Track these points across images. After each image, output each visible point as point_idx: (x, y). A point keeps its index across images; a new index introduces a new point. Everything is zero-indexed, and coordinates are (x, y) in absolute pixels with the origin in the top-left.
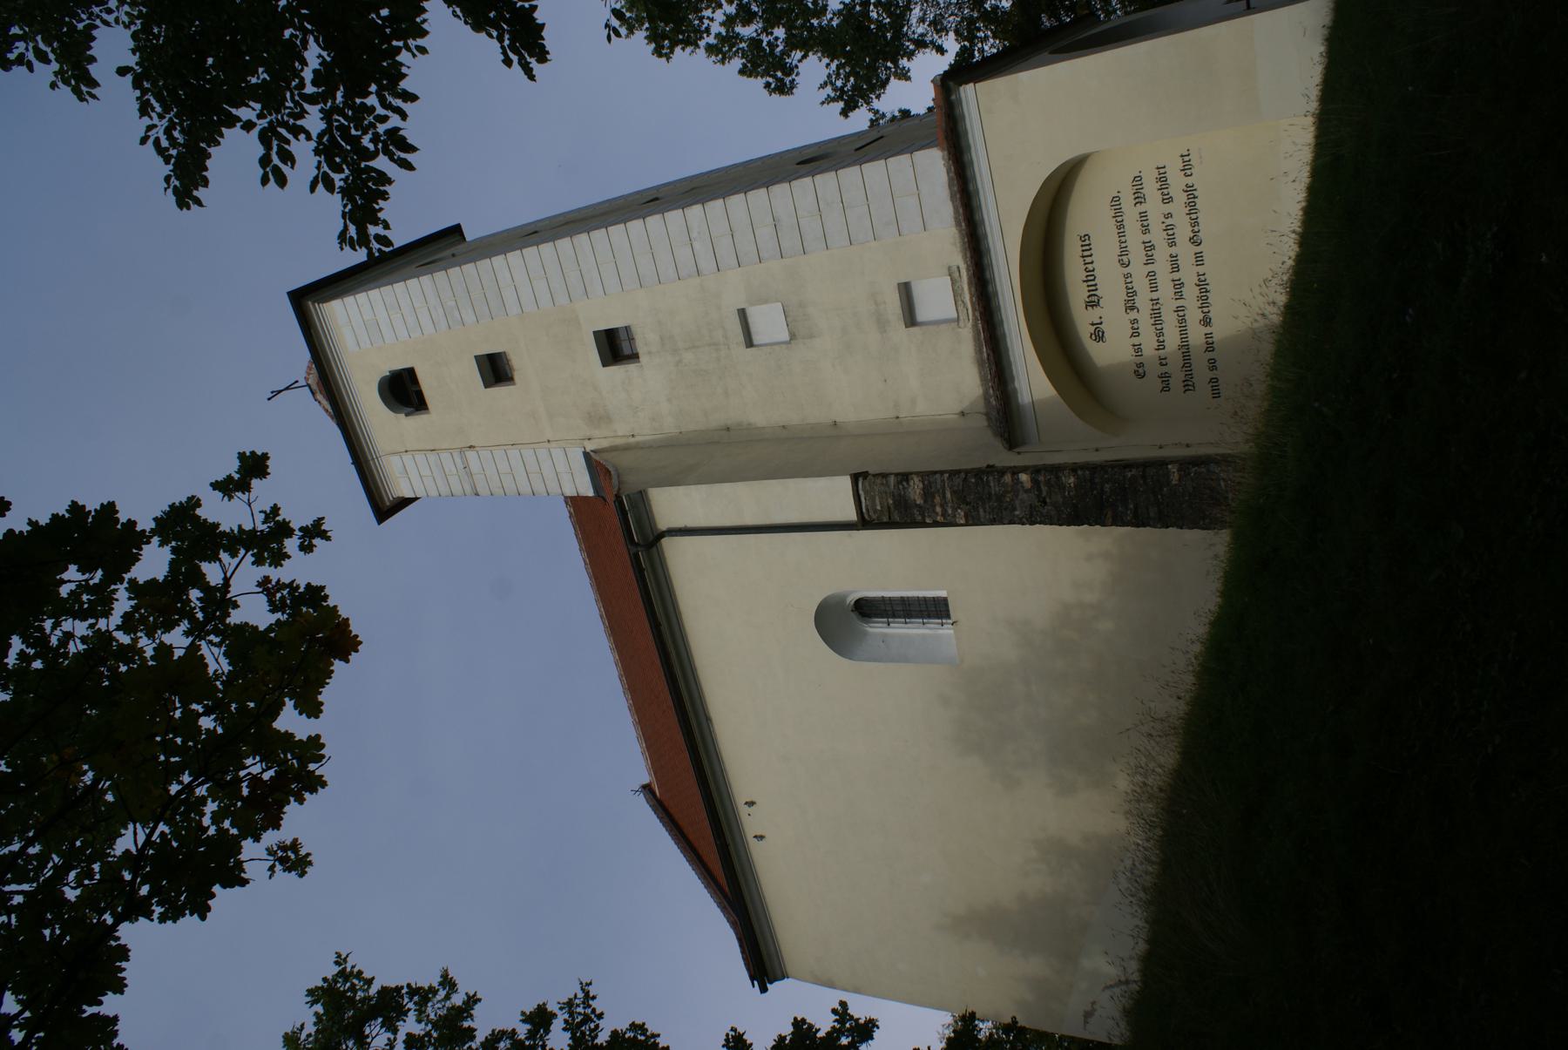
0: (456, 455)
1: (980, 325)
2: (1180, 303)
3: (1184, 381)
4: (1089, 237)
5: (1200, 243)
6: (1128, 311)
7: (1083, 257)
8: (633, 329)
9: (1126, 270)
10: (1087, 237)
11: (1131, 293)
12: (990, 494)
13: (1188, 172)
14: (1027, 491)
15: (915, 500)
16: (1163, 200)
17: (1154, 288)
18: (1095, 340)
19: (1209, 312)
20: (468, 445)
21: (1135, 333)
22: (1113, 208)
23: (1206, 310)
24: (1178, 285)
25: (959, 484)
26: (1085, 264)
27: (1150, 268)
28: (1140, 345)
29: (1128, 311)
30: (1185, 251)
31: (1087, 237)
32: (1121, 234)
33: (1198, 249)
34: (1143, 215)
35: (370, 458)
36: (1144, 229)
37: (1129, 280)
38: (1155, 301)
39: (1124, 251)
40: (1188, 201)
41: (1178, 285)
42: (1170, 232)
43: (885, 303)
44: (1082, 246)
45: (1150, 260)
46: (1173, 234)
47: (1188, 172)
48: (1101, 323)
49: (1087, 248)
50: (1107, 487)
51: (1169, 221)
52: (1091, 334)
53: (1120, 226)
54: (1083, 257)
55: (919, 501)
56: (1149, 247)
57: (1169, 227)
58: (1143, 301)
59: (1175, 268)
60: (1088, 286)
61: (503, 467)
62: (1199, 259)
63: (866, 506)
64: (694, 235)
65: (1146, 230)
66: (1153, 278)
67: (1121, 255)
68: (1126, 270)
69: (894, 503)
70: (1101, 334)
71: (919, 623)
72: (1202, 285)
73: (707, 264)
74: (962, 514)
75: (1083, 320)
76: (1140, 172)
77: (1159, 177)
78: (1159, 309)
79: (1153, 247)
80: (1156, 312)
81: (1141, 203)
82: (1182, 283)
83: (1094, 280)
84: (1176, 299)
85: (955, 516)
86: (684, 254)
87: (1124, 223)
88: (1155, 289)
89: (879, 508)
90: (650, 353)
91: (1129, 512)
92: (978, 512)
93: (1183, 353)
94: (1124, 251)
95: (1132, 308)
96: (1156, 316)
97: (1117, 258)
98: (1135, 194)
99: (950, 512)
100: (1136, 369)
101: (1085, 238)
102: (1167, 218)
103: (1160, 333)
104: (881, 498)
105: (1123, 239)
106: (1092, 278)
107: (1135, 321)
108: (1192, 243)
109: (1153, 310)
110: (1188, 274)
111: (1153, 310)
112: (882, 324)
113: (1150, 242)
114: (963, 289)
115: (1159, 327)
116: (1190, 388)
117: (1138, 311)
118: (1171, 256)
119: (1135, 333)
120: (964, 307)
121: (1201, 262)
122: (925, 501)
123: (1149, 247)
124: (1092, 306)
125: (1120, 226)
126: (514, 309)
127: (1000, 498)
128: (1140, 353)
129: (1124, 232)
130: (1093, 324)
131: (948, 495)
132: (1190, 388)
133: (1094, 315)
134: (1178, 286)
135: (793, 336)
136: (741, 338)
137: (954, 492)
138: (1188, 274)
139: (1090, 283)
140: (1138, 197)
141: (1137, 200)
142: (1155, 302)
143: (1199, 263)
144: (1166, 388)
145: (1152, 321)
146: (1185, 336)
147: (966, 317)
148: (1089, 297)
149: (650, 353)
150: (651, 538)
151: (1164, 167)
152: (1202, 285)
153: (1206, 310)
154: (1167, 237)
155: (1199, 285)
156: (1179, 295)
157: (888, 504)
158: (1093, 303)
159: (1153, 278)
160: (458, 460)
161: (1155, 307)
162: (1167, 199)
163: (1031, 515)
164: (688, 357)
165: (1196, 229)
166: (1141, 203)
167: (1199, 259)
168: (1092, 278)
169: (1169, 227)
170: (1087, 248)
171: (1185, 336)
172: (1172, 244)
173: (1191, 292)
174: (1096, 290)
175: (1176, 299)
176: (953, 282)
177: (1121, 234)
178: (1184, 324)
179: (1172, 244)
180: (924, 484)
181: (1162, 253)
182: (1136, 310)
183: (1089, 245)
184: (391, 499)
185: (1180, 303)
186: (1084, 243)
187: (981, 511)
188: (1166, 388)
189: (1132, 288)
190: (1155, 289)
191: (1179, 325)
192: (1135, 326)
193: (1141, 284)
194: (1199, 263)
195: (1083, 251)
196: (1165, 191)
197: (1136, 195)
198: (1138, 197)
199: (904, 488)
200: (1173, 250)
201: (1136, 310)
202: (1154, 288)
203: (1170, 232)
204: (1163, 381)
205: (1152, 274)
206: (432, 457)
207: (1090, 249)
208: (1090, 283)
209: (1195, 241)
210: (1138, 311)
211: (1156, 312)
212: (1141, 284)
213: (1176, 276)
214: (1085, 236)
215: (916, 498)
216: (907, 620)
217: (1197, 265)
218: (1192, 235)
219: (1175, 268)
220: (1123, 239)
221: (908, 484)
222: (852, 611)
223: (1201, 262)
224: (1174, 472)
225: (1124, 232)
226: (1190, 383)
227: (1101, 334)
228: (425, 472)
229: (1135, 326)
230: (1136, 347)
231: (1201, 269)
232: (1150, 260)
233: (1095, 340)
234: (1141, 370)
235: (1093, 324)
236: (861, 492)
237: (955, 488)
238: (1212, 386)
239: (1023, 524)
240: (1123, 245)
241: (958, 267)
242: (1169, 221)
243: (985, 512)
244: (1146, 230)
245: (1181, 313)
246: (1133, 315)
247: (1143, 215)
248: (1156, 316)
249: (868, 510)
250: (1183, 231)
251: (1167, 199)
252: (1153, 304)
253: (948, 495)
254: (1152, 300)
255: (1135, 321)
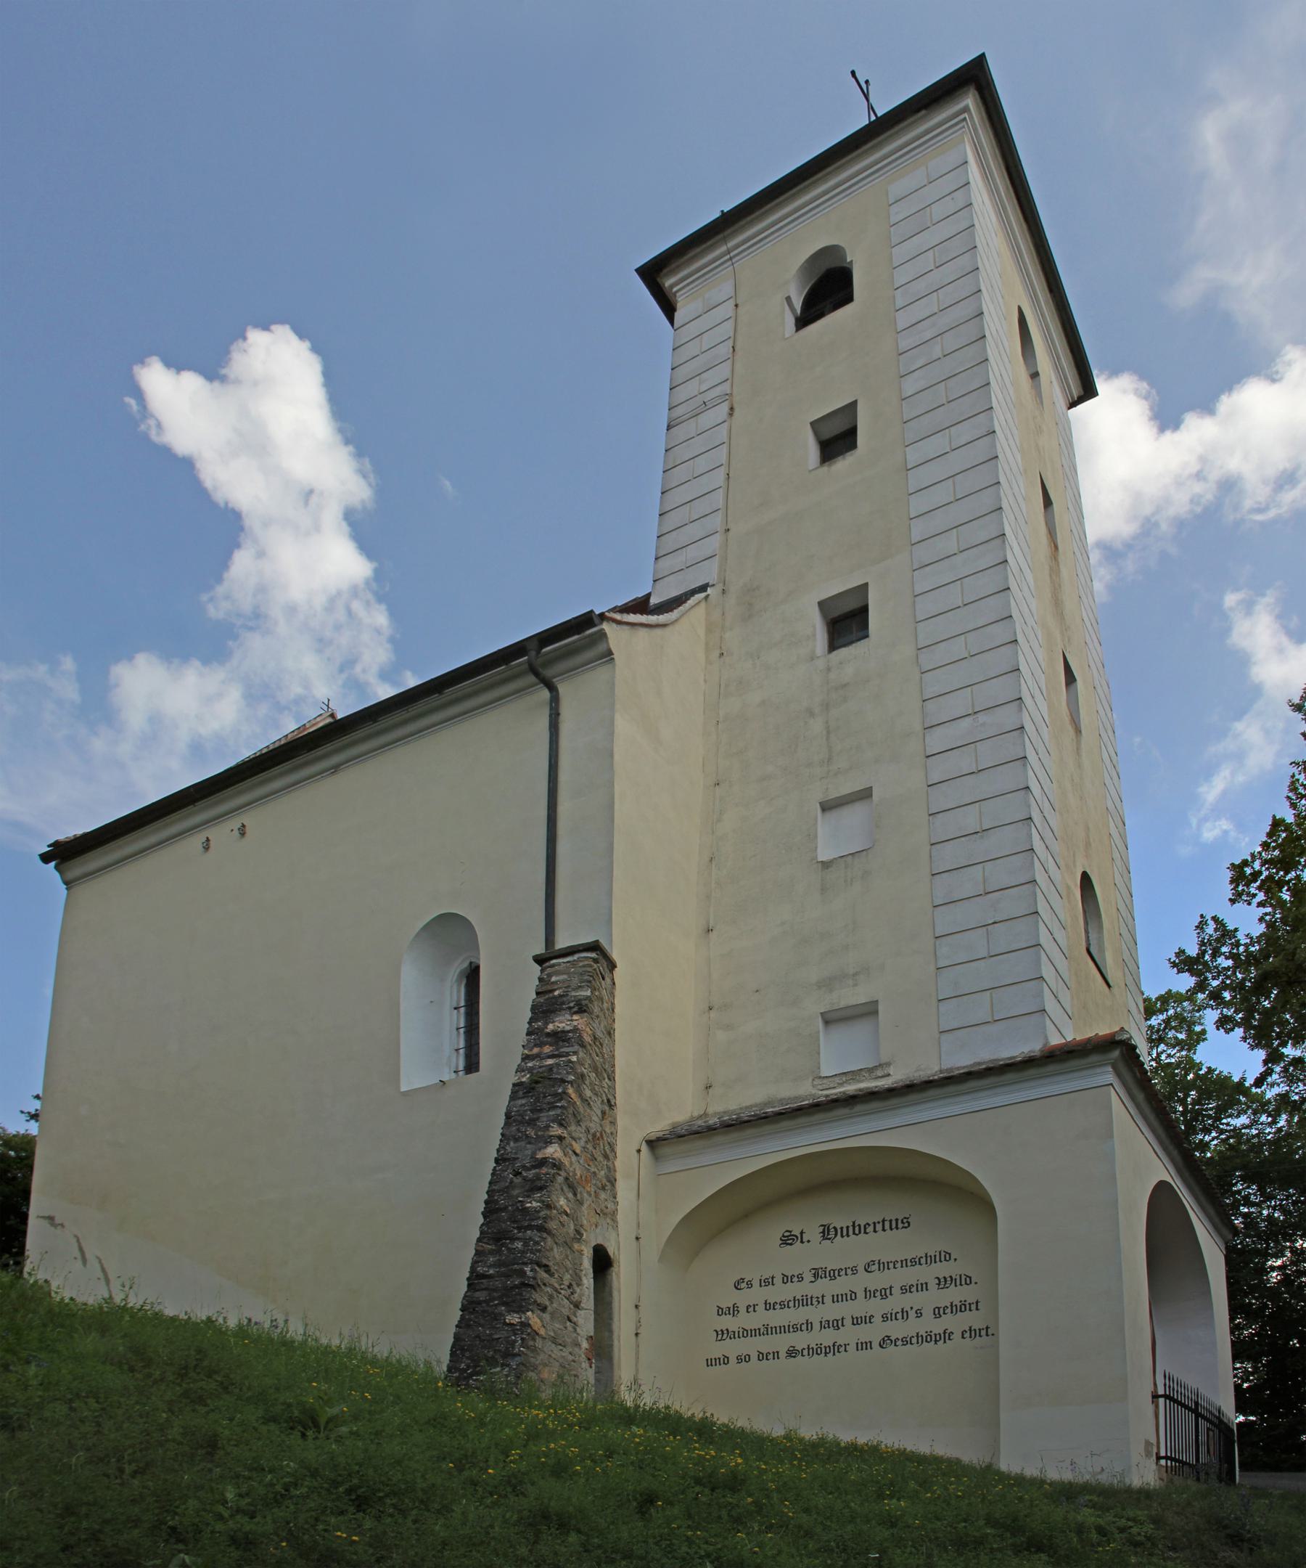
0: (726, 388)
1: (807, 1102)
2: (816, 1326)
3: (727, 1330)
4: (906, 1227)
5: (882, 1347)
6: (813, 1272)
7: (883, 1221)
8: (866, 640)
9: (861, 1269)
10: (905, 1221)
11: (833, 1275)
12: (541, 1111)
13: (967, 1335)
14: (534, 1153)
15: (553, 1022)
16: (939, 1308)
17: (836, 1299)
18: (783, 1236)
19: (802, 1355)
20: (735, 406)
21: (786, 1279)
22: (937, 1254)
23: (805, 1352)
24: (837, 1324)
25: (560, 1074)
26: (874, 1223)
27: (861, 1295)
28: (773, 1284)
29: (813, 1272)
30: (874, 1332)
31: (906, 1225)
32: (904, 1263)
33: (875, 1345)
34: (924, 1287)
35: (730, 244)
36: (908, 1288)
37: (849, 1272)
38: (821, 1300)
39: (883, 1266)
40: (932, 1334)
41: (837, 1324)
42: (899, 1316)
43: (855, 985)
44: (897, 1220)
45: (869, 1294)
46: (896, 1319)
47: (967, 1335)
48: (802, 1242)
49: (894, 1226)
50: (519, 1245)
51: (912, 1314)
52: (790, 1232)
53: (915, 1262)
54: (883, 1221)
55: (551, 1027)
56: (885, 1293)
57: (905, 1314)
58: (825, 1287)
59: (856, 1321)
60: (848, 1227)
61: (702, 464)
62: (864, 1346)
63: (559, 964)
64: (982, 718)
65: (906, 1290)
66: (849, 1298)
67: (879, 1263)
68: (861, 1269)
69: (555, 997)
70: (790, 1242)
71: (458, 1044)
72: (836, 1348)
73: (937, 741)
74: (524, 1080)
75: (807, 1220)
76: (976, 1283)
77: (967, 1303)
78: (812, 1304)
79: (884, 1297)
80: (809, 1300)
81: (939, 1284)
82: (839, 1328)
83: (854, 1233)
84: (821, 1322)
85: (523, 1071)
86: (959, 704)
87: (917, 1266)
88: (835, 1299)
89: (553, 979)
90: (829, 669)
91: (485, 1269)
92: (523, 1098)
93: (759, 1329)
94: (883, 1266)
95: (816, 1276)
96: (805, 1301)
97: (876, 1259)
98: (951, 1277)
99: (530, 1065)
100: (746, 1280)
101: (906, 1223)
102: (916, 1313)
103: (783, 1305)
104: (563, 981)
105: (898, 1265)
106: (857, 1232)
107: (801, 1278)
108: (883, 1339)
109: (812, 1298)
110: (848, 1335)
111: (812, 1298)
112: (827, 984)
113: (891, 1294)
114: (862, 1081)
115: (791, 1304)
116: (720, 1337)
117: (811, 1282)
118: (871, 1317)
119: (786, 1279)
120: (838, 1084)
121: (860, 1348)
122: (548, 1035)
123: (885, 1293)
124: (823, 1232)
125: (915, 1262)
126: (913, 456)
127: (532, 1122)
128: (763, 1284)
129: (907, 1266)
130: (802, 1233)
131: (550, 1062)
132: (720, 1337)
133: (813, 1233)
134: (835, 1325)
135: (826, 865)
136: (834, 794)
137: (550, 1068)
138: (848, 1335)
139: (851, 1229)
140: (946, 1281)
141: (942, 1280)
142: (820, 1300)
143: (860, 1345)
144: (720, 1311)
145: (799, 1297)
146: (778, 1331)
147: (825, 1086)
148: (835, 1228)
149: (829, 669)
150: (548, 673)
151: (977, 1309)
152: (836, 1348)
153: (805, 1352)
154: (894, 1312)
155: (834, 1345)
156: (825, 1325)
157: (555, 990)
158: (827, 1233)
159: (849, 1298)
160: (718, 391)
161: (814, 1300)
162: (938, 1312)
163: (505, 1160)
164: (817, 726)
165: (899, 1343)
166: (939, 1284)
167: (864, 1346)
168: (857, 1232)
169: (905, 1314)
170: (894, 1226)
171: (778, 1331)
172: (885, 1318)
173: (828, 1337)
174: (842, 1236)
175: (821, 1322)
176: (870, 1070)
177: (904, 1263)
178: (791, 1330)
179: (885, 1318)
180: (569, 1032)
181: (877, 1307)
182: (813, 1279)
183: (897, 1228)
184: (675, 289)
185: (816, 1326)
186: (900, 1221)
187: (523, 1101)
188: (720, 1311)
189: (839, 1275)
190: (835, 1299)
191: (791, 1324)
192: (795, 1279)
193: (841, 1285)
194: (860, 1345)
195: (891, 1221)
196: (948, 1310)
197: (949, 1279)
198: (946, 1281)
199: (570, 1008)
200: (877, 1319)
201: (813, 1279)
202: (836, 1299)
203: (899, 1316)
204: (729, 1308)
205: (853, 1296)
206: (725, 350)
207: (891, 1229)
208: (851, 1229)
209: (885, 1341)
210: (811, 1282)
211: (809, 1300)
212: (841, 1285)
213: (848, 1322)
214: (909, 1223)
215: (557, 1024)
216: (462, 1031)
217: (857, 1344)
218: (893, 1338)
219: (856, 1321)
220: (898, 1265)
221: (576, 1013)
222: (471, 963)
223: (860, 1348)
224: (520, 1318)
225: (907, 1266)
226: (725, 1336)
227: (790, 1242)
228: (707, 341)
229: (795, 1279)
230: (770, 1280)
231: (852, 1348)
232: (869, 1294)
233: (783, 1236)
234: (743, 1285)
235: (802, 1233)
236: (576, 957)
237: (555, 1070)
238: (719, 1359)
239: (498, 1151)
240: (891, 1265)
241: (889, 1075)
242: (912, 1314)
243: (521, 1105)
244: (906, 1290)
245: (804, 1327)
246: (808, 1277)
247: (924, 1287)
248: (805, 1301)
249: (553, 966)
250: (897, 1329)
251: (938, 1312)
252: (818, 1298)
253: (550, 1062)
254: (823, 1296)
255: (800, 1278)
